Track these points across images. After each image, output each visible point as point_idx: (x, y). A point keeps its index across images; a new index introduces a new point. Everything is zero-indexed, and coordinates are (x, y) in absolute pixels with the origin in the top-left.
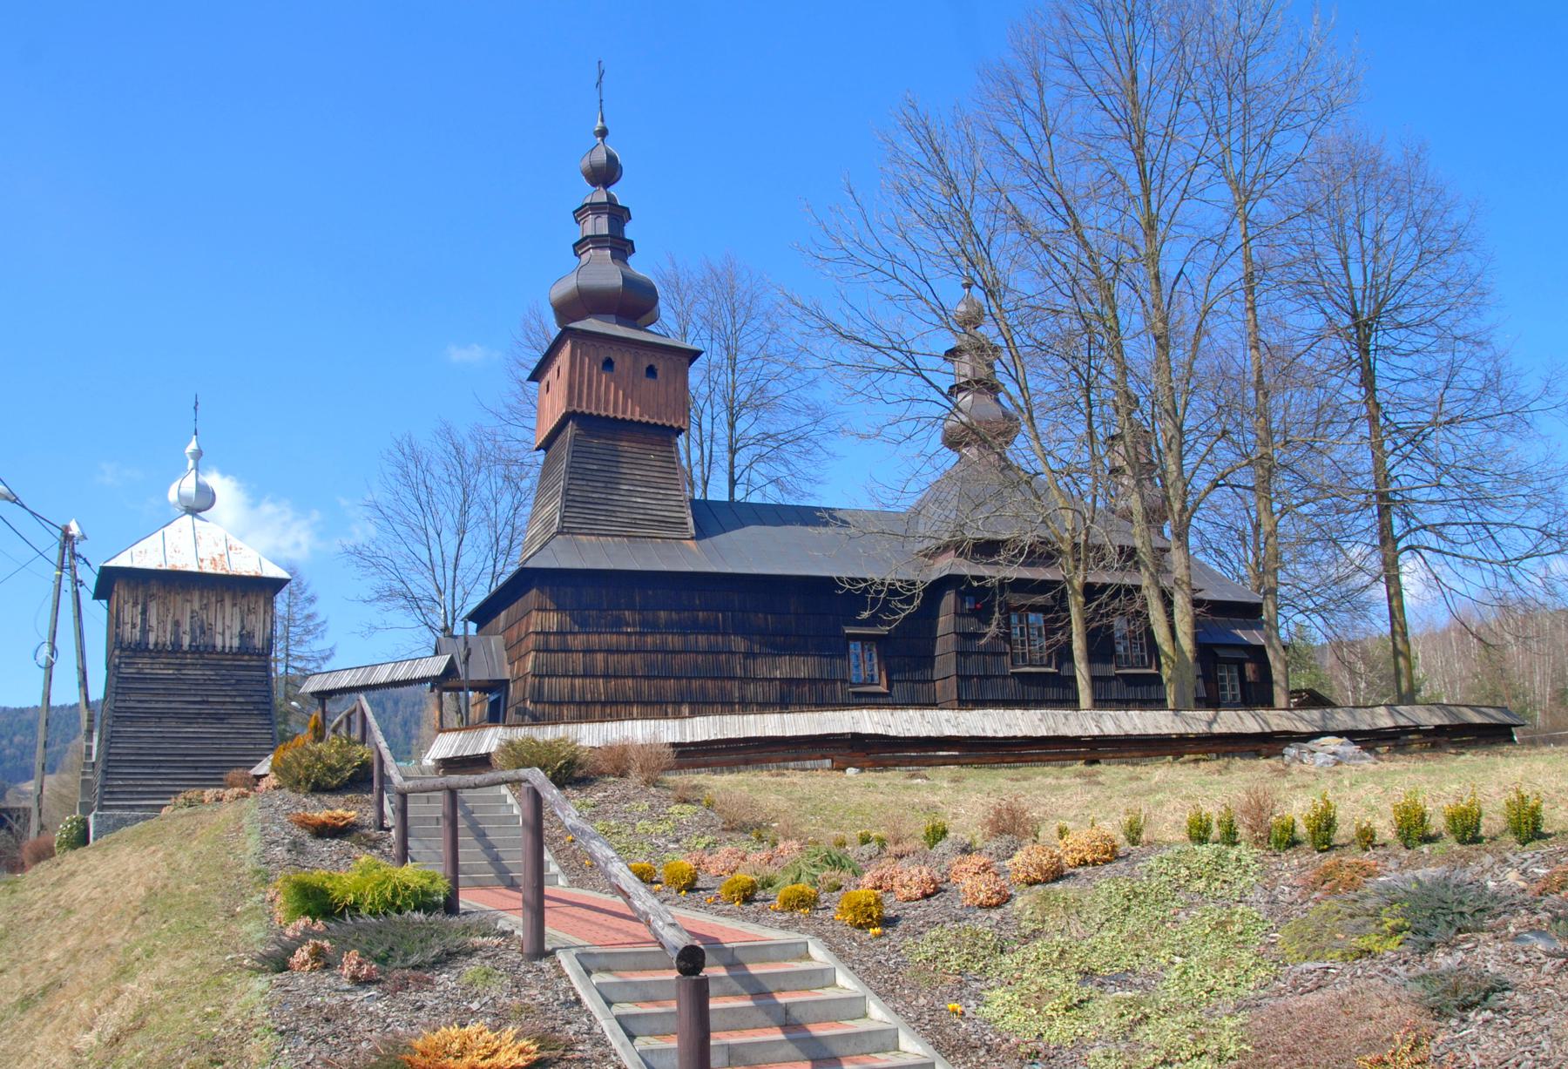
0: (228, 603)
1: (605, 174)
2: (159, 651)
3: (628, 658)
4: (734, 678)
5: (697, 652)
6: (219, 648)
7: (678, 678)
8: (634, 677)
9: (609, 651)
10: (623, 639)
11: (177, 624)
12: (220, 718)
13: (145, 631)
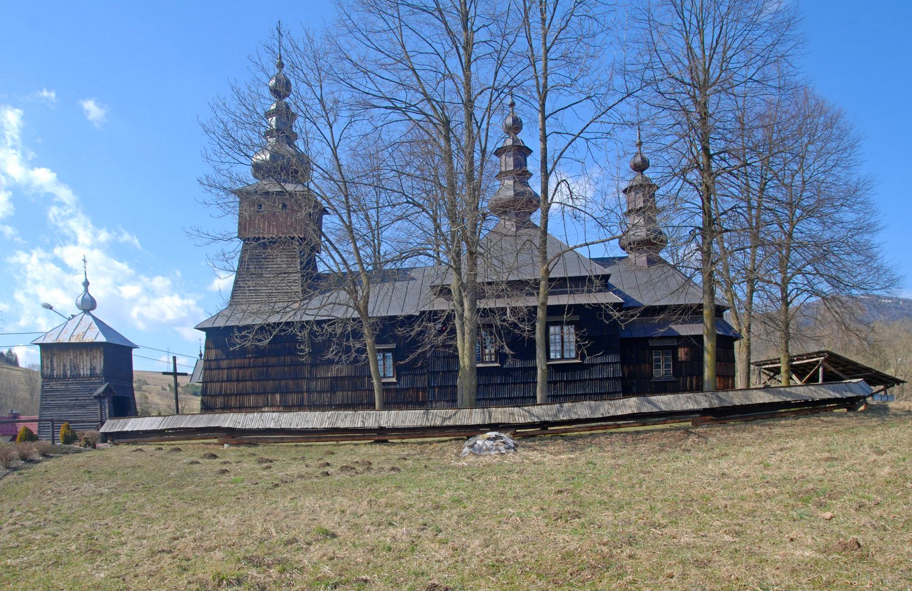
0: (85, 354)
1: (641, 167)
2: (58, 378)
3: (249, 371)
4: (304, 378)
5: (285, 366)
7: (275, 380)
8: (252, 380)
9: (240, 368)
10: (247, 361)
11: (64, 366)
12: (83, 407)
13: (52, 370)
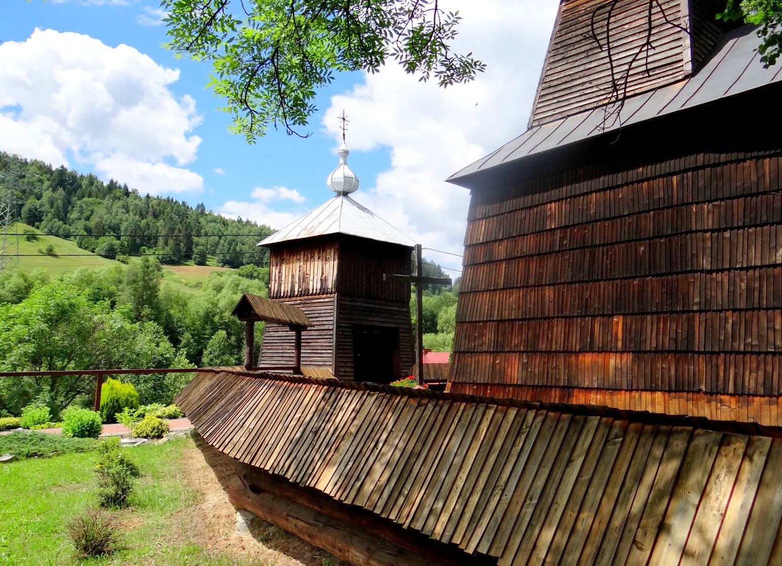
6: (311, 292)
10: (545, 240)
